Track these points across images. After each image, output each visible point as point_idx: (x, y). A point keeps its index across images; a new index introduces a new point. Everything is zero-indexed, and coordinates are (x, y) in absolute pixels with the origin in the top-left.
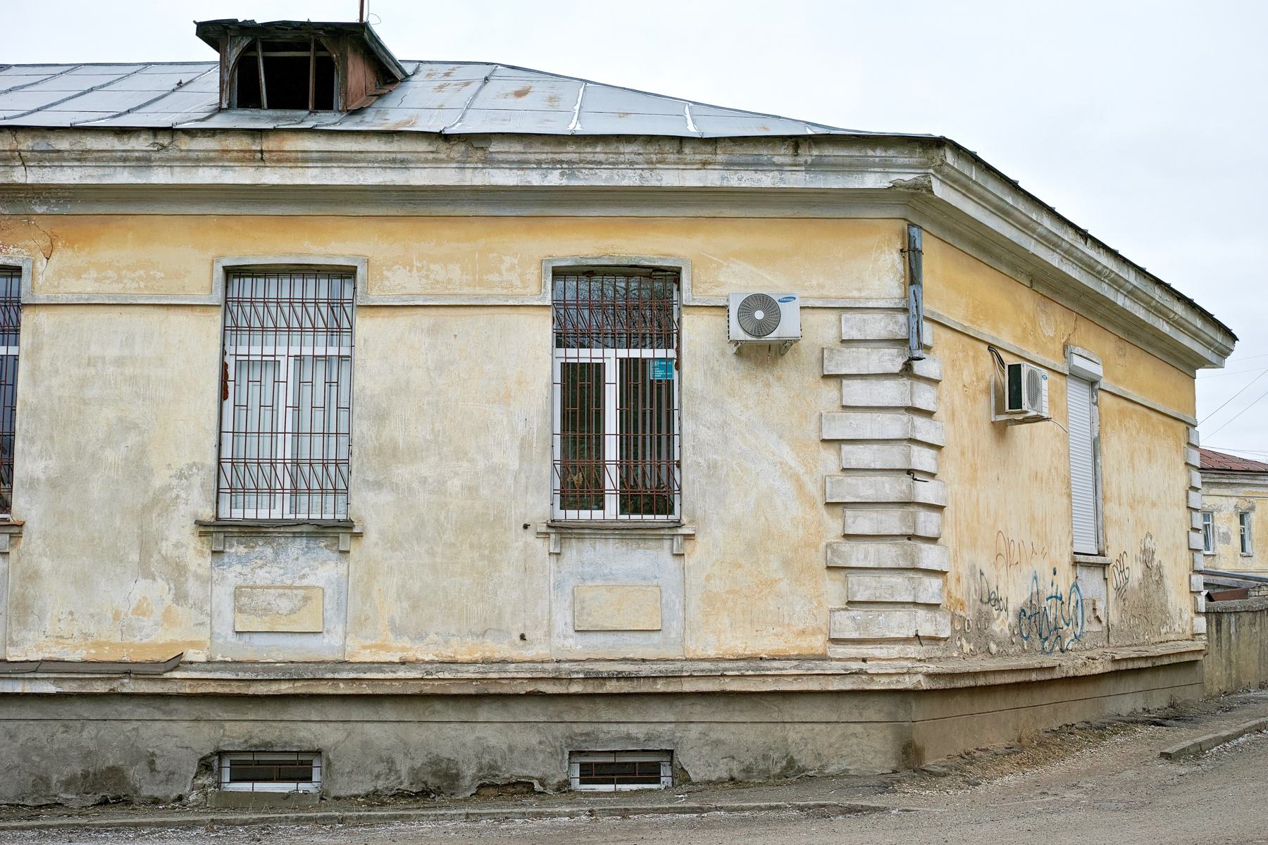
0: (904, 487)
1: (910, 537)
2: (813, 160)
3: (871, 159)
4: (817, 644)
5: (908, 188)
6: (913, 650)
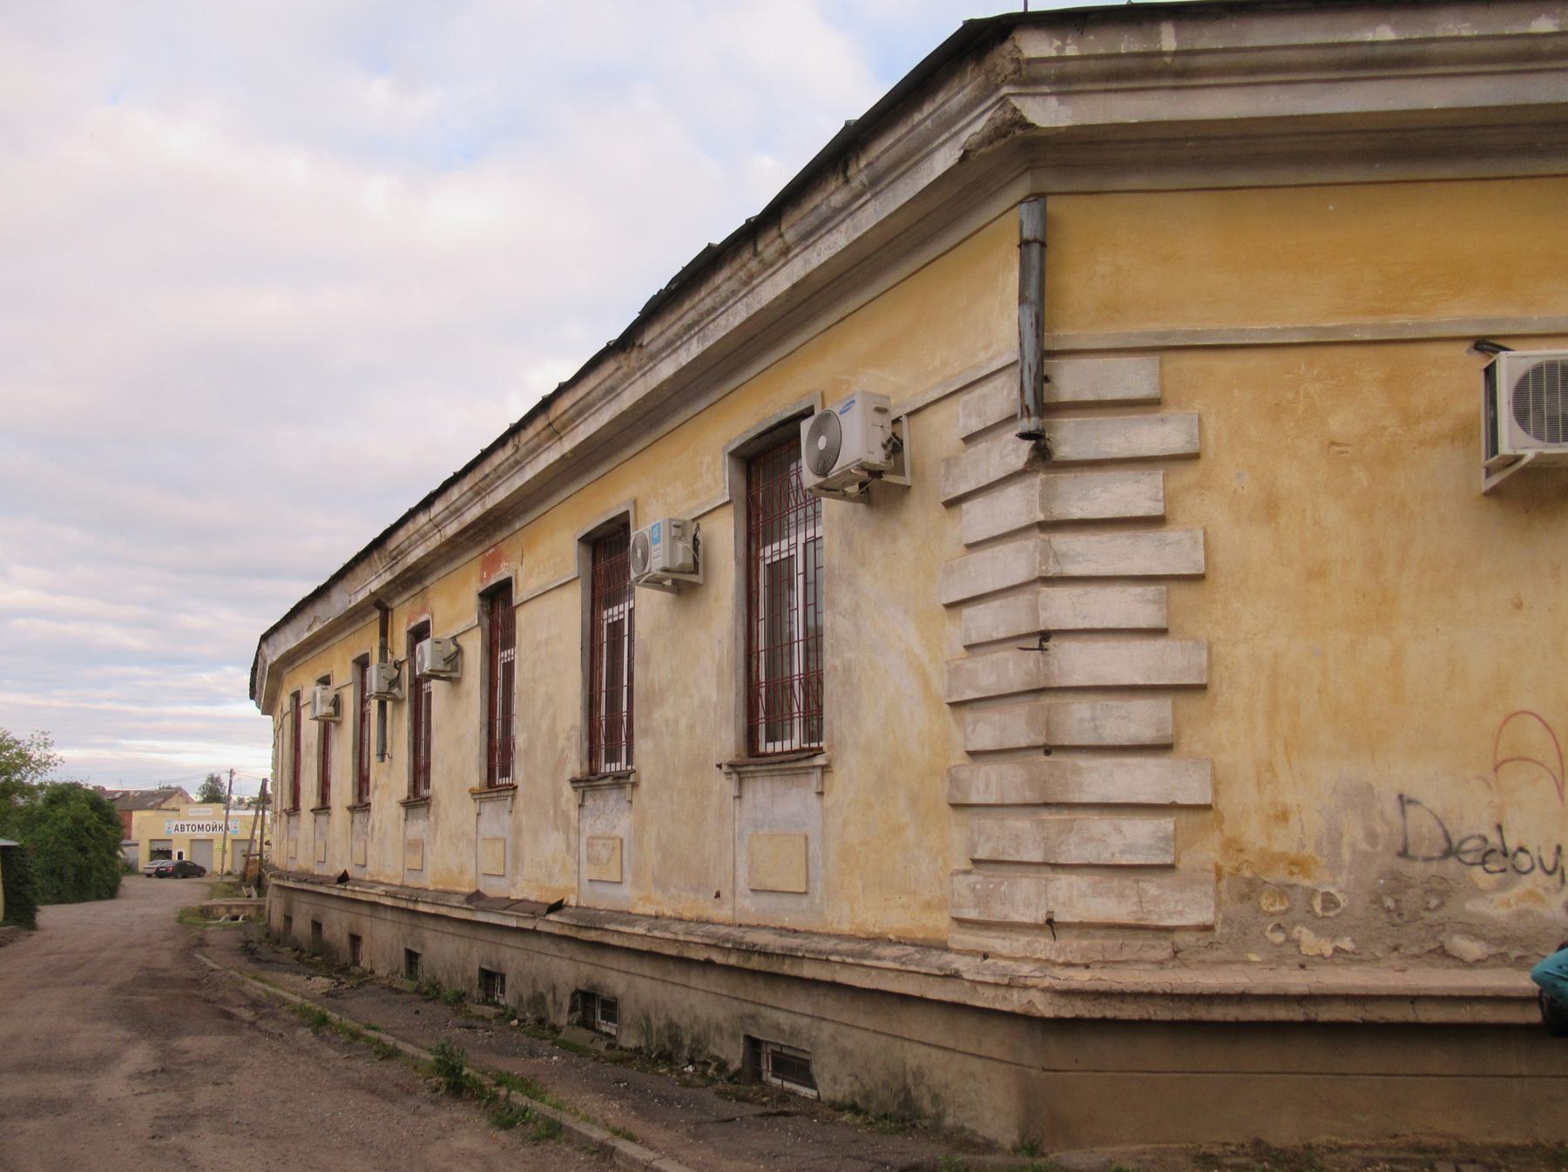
0: (1031, 664)
1: (1048, 750)
2: (867, 175)
3: (922, 127)
4: (938, 923)
5: (991, 142)
6: (1044, 946)
